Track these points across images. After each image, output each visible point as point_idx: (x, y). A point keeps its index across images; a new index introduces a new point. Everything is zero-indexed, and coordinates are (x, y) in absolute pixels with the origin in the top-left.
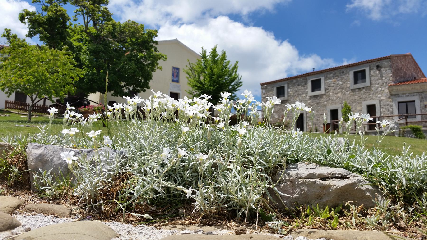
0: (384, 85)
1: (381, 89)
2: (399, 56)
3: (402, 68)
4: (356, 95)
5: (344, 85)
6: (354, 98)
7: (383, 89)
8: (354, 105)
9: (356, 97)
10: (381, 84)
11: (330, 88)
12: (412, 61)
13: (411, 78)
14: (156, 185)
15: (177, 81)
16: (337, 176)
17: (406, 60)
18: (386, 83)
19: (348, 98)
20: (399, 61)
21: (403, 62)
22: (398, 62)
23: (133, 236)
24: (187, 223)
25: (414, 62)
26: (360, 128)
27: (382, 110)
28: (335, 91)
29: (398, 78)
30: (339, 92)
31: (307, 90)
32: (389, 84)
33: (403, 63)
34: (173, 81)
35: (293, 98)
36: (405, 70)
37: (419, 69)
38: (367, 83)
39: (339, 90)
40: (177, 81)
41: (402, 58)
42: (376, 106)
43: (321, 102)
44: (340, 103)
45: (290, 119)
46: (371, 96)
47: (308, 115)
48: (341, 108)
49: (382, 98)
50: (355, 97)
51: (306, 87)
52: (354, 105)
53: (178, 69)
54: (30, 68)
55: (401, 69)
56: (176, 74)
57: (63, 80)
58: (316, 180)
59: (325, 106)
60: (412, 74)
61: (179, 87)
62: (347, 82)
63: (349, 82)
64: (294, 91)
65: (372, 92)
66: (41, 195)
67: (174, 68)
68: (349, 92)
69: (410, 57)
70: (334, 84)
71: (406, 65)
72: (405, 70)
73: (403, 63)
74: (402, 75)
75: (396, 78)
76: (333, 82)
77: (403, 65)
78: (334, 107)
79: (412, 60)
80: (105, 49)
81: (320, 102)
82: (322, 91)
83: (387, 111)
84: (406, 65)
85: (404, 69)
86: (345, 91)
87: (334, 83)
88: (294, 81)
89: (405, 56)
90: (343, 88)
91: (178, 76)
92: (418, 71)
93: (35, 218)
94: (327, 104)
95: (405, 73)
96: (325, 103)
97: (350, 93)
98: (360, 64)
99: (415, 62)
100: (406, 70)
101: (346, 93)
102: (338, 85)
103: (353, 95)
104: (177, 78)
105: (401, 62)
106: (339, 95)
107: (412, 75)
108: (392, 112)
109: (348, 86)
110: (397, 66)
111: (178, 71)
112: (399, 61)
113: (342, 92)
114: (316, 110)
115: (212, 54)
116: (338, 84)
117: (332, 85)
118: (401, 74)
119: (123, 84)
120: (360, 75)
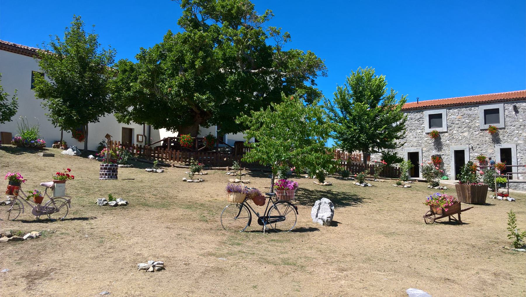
1: (518, 132)
5: (472, 123)
7: (520, 132)
11: (454, 125)
14: (442, 181)
19: (477, 139)
23: (262, 295)
24: (22, 274)
27: (518, 155)
28: (460, 130)
30: (465, 131)
46: (505, 138)
47: (424, 154)
49: (519, 142)
51: (421, 122)
62: (475, 121)
65: (507, 135)
68: (477, 132)
70: (459, 122)
76: (457, 119)
78: (459, 148)
86: (473, 131)
87: (458, 121)
90: (470, 127)
93: (470, 101)
98: (489, 102)
102: (464, 123)
103: (483, 136)
106: (466, 134)
109: (477, 125)
117: (457, 122)
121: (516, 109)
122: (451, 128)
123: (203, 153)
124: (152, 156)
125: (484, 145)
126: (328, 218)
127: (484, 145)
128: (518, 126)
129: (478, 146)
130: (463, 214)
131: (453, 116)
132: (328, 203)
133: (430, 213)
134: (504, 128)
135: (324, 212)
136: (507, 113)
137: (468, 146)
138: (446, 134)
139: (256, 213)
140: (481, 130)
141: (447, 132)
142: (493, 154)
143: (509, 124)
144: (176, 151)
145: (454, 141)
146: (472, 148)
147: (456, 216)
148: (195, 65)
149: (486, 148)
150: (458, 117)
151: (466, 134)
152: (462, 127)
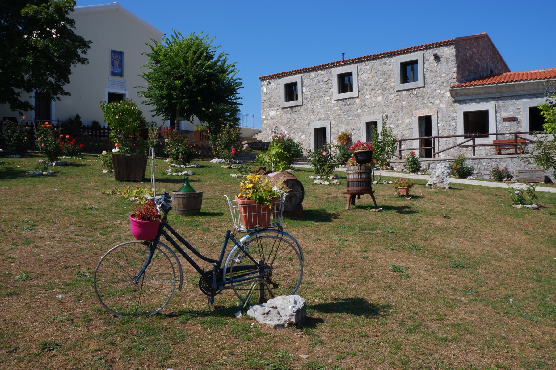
0: (445, 85)
2: (468, 39)
3: (472, 57)
4: (404, 100)
5: (387, 83)
7: (442, 92)
8: (401, 115)
9: (404, 103)
10: (440, 83)
11: (366, 87)
12: (488, 45)
13: (487, 72)
15: (121, 75)
16: (117, 170)
17: (478, 44)
18: (448, 82)
20: (468, 47)
21: (475, 48)
22: (466, 49)
25: (491, 47)
27: (439, 125)
28: (373, 93)
29: (465, 75)
31: (331, 90)
32: (452, 85)
33: (474, 50)
34: (113, 74)
35: (310, 102)
36: (477, 61)
37: (498, 57)
39: (379, 92)
40: (121, 75)
41: (472, 41)
42: (432, 117)
43: (352, 109)
45: (306, 136)
46: (425, 101)
50: (402, 104)
52: (401, 115)
53: (121, 54)
55: (471, 59)
56: (117, 62)
58: (70, 28)
59: (359, 116)
60: (487, 65)
61: (122, 84)
62: (390, 79)
63: (393, 80)
64: (312, 90)
67: (113, 52)
68: (393, 96)
69: (486, 39)
71: (478, 53)
72: (477, 61)
73: (474, 50)
74: (472, 68)
75: (462, 74)
76: (369, 79)
77: (473, 53)
78: (371, 119)
79: (489, 43)
82: (354, 93)
83: (448, 125)
84: (478, 53)
85: (475, 59)
86: (388, 94)
87: (371, 80)
88: (312, 74)
89: (477, 38)
90: (385, 89)
91: (121, 65)
92: (498, 61)
94: (362, 114)
95: (477, 65)
96: (359, 111)
97: (395, 96)
99: (494, 47)
100: (479, 60)
101: (390, 96)
102: (378, 84)
104: (120, 69)
105: (471, 48)
106: (380, 99)
107: (487, 67)
108: (455, 129)
110: (465, 55)
111: (121, 57)
112: (468, 47)
113: (383, 94)
114: (345, 122)
118: (471, 66)
120: (409, 68)
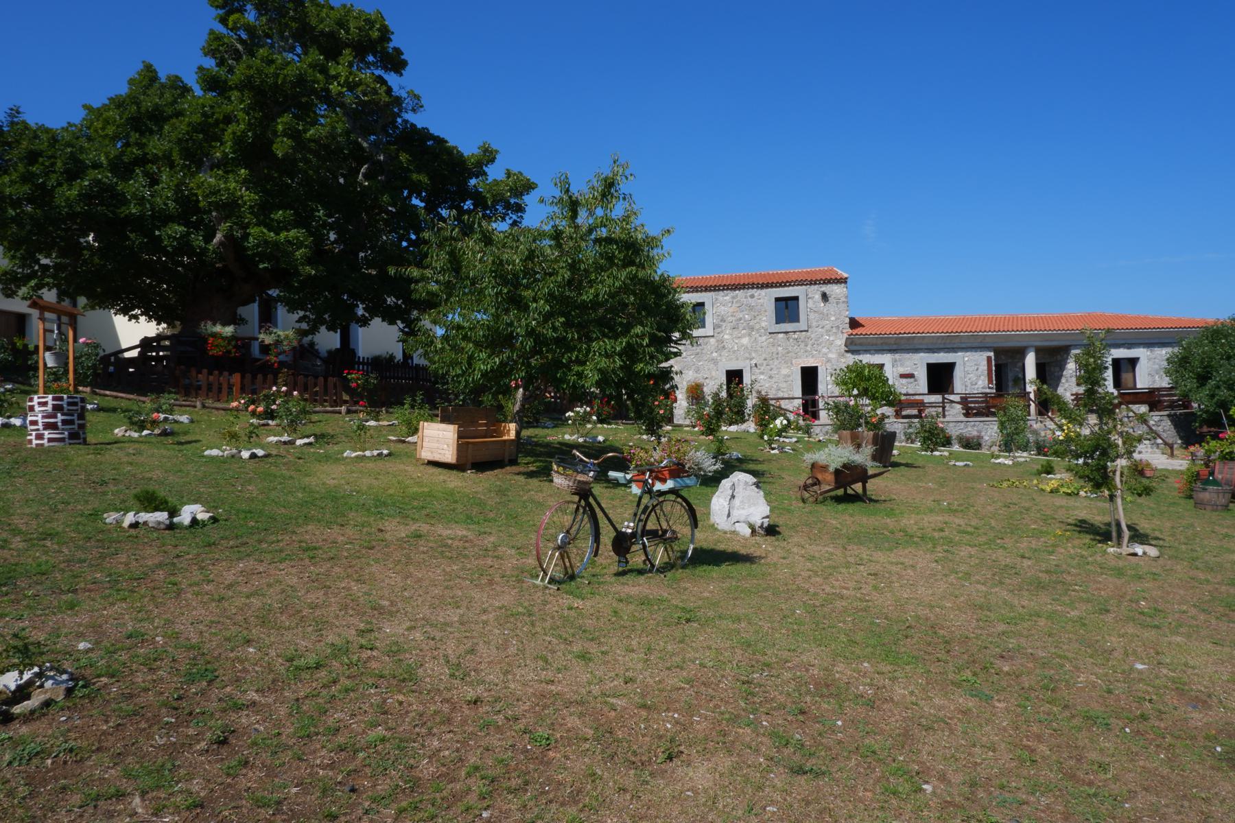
4: (779, 345)
6: (774, 350)
7: (831, 339)
11: (724, 324)
26: (435, 322)
28: (736, 333)
30: (744, 336)
38: (802, 325)
42: (819, 368)
43: (704, 352)
44: (747, 358)
48: (749, 368)
54: (465, 314)
57: (231, 55)
62: (760, 317)
66: (281, 551)
70: (734, 318)
80: (24, 595)
81: (702, 353)
87: (732, 316)
90: (752, 329)
106: (745, 341)
115: (455, 152)
116: (740, 319)
117: (730, 319)
119: (282, 294)
121: (825, 297)
122: (720, 330)
123: (260, 376)
124: (559, 398)
125: (775, 360)
126: (763, 518)
127: (775, 360)
128: (828, 327)
129: (765, 362)
130: (871, 484)
131: (723, 308)
132: (750, 483)
133: (810, 481)
134: (807, 331)
135: (749, 507)
136: (810, 304)
137: (748, 361)
138: (712, 340)
139: (573, 516)
140: (770, 333)
141: (713, 336)
142: (789, 376)
143: (814, 324)
144: (221, 374)
145: (725, 353)
146: (756, 365)
147: (858, 487)
148: (136, 132)
149: (779, 366)
150: (731, 310)
151: (745, 341)
152: (738, 328)
